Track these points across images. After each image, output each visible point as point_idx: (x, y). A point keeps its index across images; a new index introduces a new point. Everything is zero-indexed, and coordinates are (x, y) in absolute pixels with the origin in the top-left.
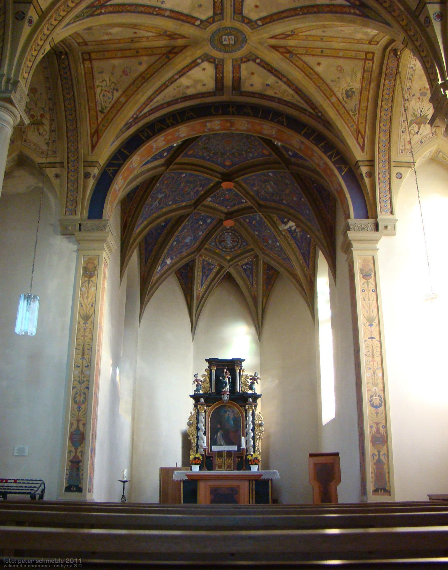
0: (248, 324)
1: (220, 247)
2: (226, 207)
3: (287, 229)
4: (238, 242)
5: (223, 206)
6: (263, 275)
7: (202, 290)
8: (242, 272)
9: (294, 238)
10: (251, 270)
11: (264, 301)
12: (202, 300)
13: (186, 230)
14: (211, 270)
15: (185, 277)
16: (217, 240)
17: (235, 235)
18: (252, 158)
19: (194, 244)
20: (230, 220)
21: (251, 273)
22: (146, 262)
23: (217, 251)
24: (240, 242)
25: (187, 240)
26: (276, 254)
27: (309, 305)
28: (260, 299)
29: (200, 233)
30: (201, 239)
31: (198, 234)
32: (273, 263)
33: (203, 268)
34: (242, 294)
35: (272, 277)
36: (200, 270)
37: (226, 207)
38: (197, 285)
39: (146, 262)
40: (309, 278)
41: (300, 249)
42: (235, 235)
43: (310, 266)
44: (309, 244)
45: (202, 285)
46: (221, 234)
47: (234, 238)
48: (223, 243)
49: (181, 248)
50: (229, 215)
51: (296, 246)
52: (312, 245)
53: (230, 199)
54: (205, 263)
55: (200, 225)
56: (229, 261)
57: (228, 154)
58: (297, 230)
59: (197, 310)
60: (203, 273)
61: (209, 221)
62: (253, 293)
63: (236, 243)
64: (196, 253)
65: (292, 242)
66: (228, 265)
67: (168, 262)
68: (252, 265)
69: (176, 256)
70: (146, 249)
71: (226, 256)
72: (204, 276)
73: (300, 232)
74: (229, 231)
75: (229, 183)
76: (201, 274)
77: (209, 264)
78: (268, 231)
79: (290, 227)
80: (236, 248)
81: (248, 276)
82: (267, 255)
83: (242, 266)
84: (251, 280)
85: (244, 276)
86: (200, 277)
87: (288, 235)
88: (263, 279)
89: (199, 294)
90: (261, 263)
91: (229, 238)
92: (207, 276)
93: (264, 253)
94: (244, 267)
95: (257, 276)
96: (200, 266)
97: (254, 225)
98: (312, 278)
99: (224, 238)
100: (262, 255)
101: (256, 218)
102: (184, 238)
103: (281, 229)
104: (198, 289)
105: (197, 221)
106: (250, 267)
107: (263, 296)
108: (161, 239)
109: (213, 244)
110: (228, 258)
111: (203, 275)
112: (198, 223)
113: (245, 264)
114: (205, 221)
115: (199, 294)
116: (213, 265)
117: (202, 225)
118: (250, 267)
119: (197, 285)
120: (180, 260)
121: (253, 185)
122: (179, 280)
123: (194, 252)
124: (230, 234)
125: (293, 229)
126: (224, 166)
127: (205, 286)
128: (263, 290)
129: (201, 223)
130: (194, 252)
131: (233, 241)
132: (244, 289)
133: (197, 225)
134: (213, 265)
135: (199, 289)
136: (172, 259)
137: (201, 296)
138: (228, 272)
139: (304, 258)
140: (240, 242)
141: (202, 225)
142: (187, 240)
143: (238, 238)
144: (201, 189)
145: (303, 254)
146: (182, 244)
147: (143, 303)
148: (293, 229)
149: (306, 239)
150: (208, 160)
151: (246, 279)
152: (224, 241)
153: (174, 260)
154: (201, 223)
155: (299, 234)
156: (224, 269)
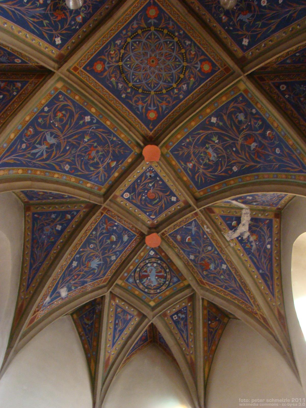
0: (182, 402)
1: (141, 286)
2: (149, 216)
3: (237, 238)
4: (165, 278)
5: (145, 213)
6: (204, 328)
7: (113, 352)
8: (172, 326)
9: (248, 251)
10: (185, 319)
11: (207, 369)
12: (111, 368)
13: (92, 246)
14: (126, 322)
15: (88, 321)
16: (137, 275)
17: (162, 267)
18: (188, 92)
19: (104, 275)
20: (155, 234)
21: (185, 325)
22: (28, 286)
23: (137, 293)
24: (169, 277)
25: (94, 264)
26: (221, 286)
27: (284, 355)
28: (200, 362)
29: (113, 258)
30: (114, 267)
31: (110, 257)
32: (218, 301)
33: (117, 317)
34: (174, 360)
35: (218, 321)
36: (112, 320)
37: (149, 216)
38: (106, 344)
39: (28, 286)
40: (276, 313)
41: (258, 269)
42: (162, 267)
43: (277, 294)
44: (270, 260)
45: (114, 344)
46: (142, 264)
47: (160, 272)
48: (144, 280)
49: (84, 276)
50: (154, 229)
51: (252, 265)
52: (274, 260)
53: (154, 199)
54: (119, 310)
55: (113, 243)
56: (153, 308)
57: (152, 93)
58: (252, 239)
59: (103, 384)
60: (116, 324)
61: (126, 238)
62: (188, 357)
63: (163, 280)
64: (106, 288)
65: (246, 258)
66: (152, 314)
67: (64, 292)
68: (186, 314)
69: (76, 287)
70: (31, 266)
71: (150, 301)
72: (270, 28)
73: (255, 241)
74: (153, 260)
75: (155, 147)
76: (112, 326)
77: (124, 311)
78: (209, 248)
79: (242, 234)
80: (164, 288)
81: (180, 331)
82: (207, 290)
83: (171, 316)
84: (185, 337)
85: (176, 331)
86: (111, 331)
87: (239, 247)
88: (204, 332)
89: (109, 358)
90: (199, 305)
91: (154, 271)
92: (121, 331)
93: (203, 288)
94: (175, 317)
95: (194, 329)
96: (112, 314)
97: (189, 244)
98: (282, 312)
99: (146, 271)
100: (202, 291)
101: (191, 230)
102: (90, 259)
103: (228, 239)
104: (107, 349)
105: (110, 233)
106: (184, 316)
107: (205, 361)
108: (54, 251)
109: (131, 280)
110: (152, 304)
111: (115, 329)
112: (109, 238)
113: (177, 313)
114: (120, 238)
115: (109, 358)
116: (130, 314)
117: (115, 243)
118: (184, 316)
119: (106, 344)
120: (82, 295)
121: (187, 159)
122: (81, 337)
123: (104, 286)
124: (155, 265)
125: (245, 237)
126: (146, 121)
127: (118, 346)
128: (205, 352)
129: (114, 238)
130: (104, 286)
131: (160, 277)
132: (175, 350)
133: (109, 241)
134: (130, 314)
135: (109, 350)
136: (69, 290)
137: (111, 361)
138: (152, 323)
139: (266, 281)
140: (169, 277)
141: (115, 243)
142: (94, 264)
143: (165, 271)
144: (113, 164)
145: (263, 276)
146: (86, 269)
147: (12, 348)
148: (245, 237)
149: (264, 252)
150: (123, 100)
151: (178, 336)
152: (147, 276)
153: (73, 294)
154: (114, 238)
155: (253, 244)
156: (146, 320)
